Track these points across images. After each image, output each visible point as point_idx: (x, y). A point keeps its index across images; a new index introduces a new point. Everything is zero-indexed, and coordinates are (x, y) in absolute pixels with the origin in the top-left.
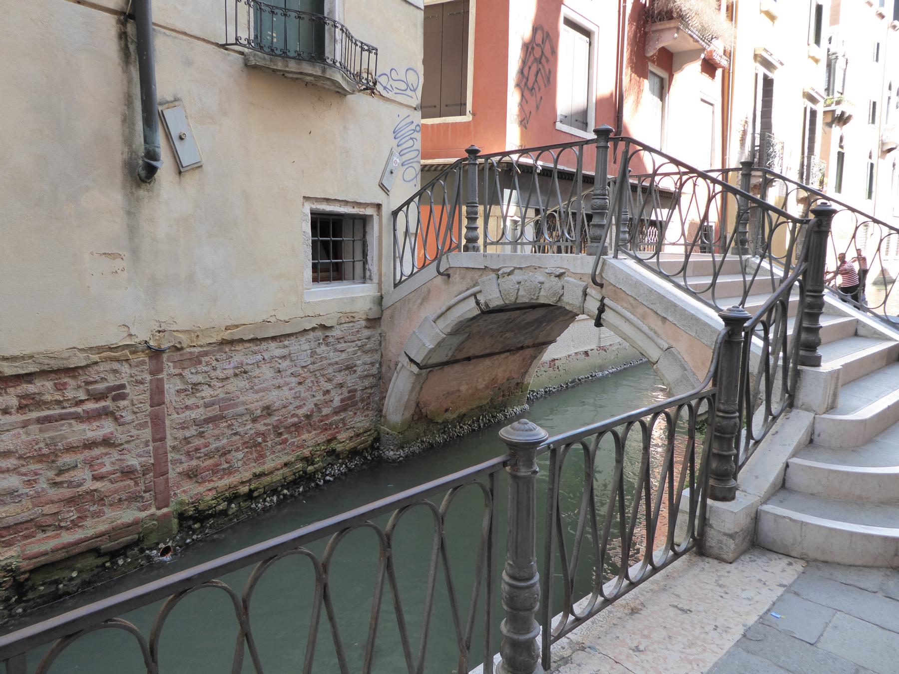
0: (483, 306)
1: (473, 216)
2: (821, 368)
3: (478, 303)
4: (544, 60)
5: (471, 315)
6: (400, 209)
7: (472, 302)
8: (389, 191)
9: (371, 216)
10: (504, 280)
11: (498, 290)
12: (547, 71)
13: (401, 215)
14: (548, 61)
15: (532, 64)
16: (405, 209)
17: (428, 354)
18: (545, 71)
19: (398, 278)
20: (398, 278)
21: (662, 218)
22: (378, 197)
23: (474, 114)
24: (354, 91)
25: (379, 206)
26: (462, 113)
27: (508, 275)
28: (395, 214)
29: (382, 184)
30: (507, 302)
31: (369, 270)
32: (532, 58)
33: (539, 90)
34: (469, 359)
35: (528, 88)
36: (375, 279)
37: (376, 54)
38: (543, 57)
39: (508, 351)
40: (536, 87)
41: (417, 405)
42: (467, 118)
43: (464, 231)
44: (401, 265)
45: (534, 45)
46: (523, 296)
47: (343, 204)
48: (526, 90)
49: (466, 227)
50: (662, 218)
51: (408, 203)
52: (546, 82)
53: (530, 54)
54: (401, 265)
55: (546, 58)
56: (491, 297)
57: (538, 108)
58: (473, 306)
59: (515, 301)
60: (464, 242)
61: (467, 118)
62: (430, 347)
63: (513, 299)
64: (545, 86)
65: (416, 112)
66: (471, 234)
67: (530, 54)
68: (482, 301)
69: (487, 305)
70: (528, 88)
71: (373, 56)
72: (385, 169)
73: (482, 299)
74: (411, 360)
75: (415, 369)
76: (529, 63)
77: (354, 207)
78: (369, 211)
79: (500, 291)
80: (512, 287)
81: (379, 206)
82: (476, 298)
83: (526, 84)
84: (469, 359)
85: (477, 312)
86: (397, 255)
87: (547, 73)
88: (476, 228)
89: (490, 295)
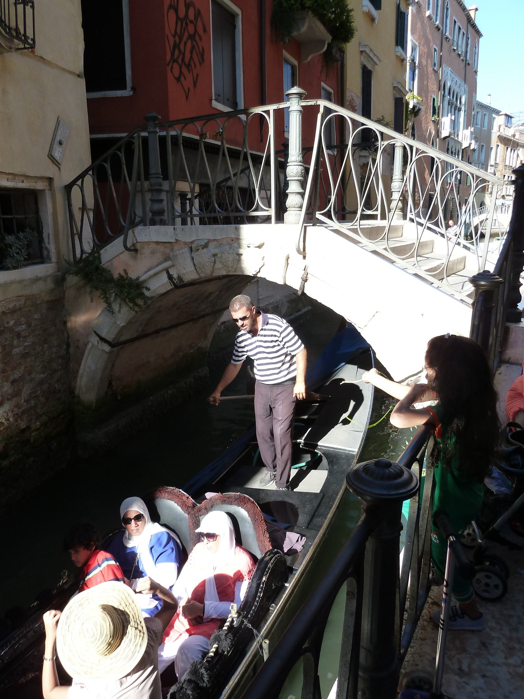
0: (176, 280)
1: (158, 188)
2: (521, 323)
3: (170, 277)
4: (197, 38)
5: (163, 291)
6: (74, 183)
7: (164, 278)
8: (59, 164)
9: (43, 191)
10: (198, 253)
11: (192, 264)
12: (201, 48)
13: (75, 190)
14: (201, 39)
15: (187, 40)
16: (79, 182)
17: (120, 332)
18: (198, 47)
19: (78, 255)
20: (78, 255)
21: (512, 164)
22: (50, 171)
23: (133, 89)
24: (11, 48)
25: (50, 180)
26: (124, 87)
27: (203, 248)
28: (68, 188)
29: (51, 155)
30: (202, 275)
31: (47, 249)
32: (186, 34)
33: (195, 66)
34: (157, 332)
35: (185, 64)
36: (54, 259)
37: (33, 7)
38: (197, 34)
39: (192, 320)
40: (192, 63)
41: (110, 384)
42: (127, 93)
43: (149, 203)
44: (81, 242)
45: (188, 21)
46: (219, 269)
47: (10, 177)
48: (183, 66)
49: (151, 200)
50: (512, 164)
51: (82, 176)
52: (201, 60)
53: (185, 30)
54: (81, 242)
55: (200, 36)
56: (184, 271)
57: (195, 84)
58: (166, 281)
59: (212, 274)
60: (150, 215)
61: (127, 93)
62: (122, 325)
63: (209, 272)
64: (200, 64)
65: (79, 79)
66: (156, 207)
67: (185, 30)
68: (175, 276)
69: (180, 278)
70: (185, 64)
71: (28, 9)
72: (53, 140)
73: (174, 273)
74: (102, 339)
75: (107, 348)
76: (185, 39)
77: (23, 181)
78: (40, 186)
79: (194, 264)
80: (207, 260)
81: (50, 180)
82: (168, 273)
83: (183, 60)
84: (157, 332)
85: (170, 287)
86: (75, 232)
87: (201, 50)
88: (161, 201)
89: (185, 269)
